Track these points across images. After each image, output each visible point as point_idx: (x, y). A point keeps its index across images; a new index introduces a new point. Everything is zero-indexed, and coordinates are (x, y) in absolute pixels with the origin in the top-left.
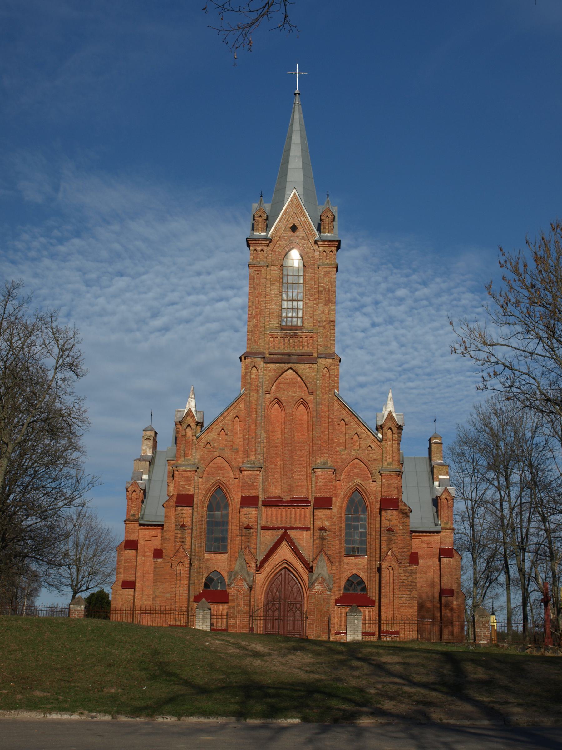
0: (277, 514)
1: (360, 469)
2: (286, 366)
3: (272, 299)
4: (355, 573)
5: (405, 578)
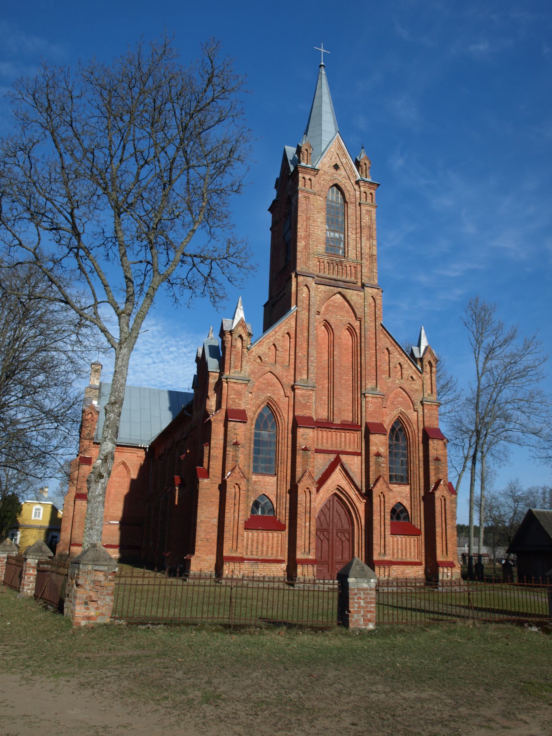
0: (327, 437)
1: (403, 398)
3: (318, 226)
4: (399, 501)
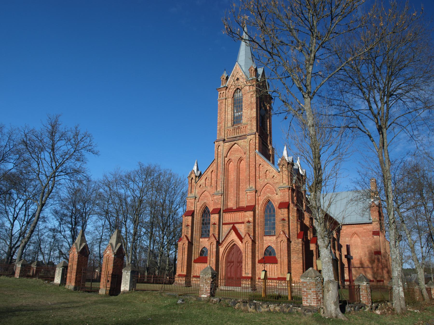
2: (233, 143)
5: (295, 247)
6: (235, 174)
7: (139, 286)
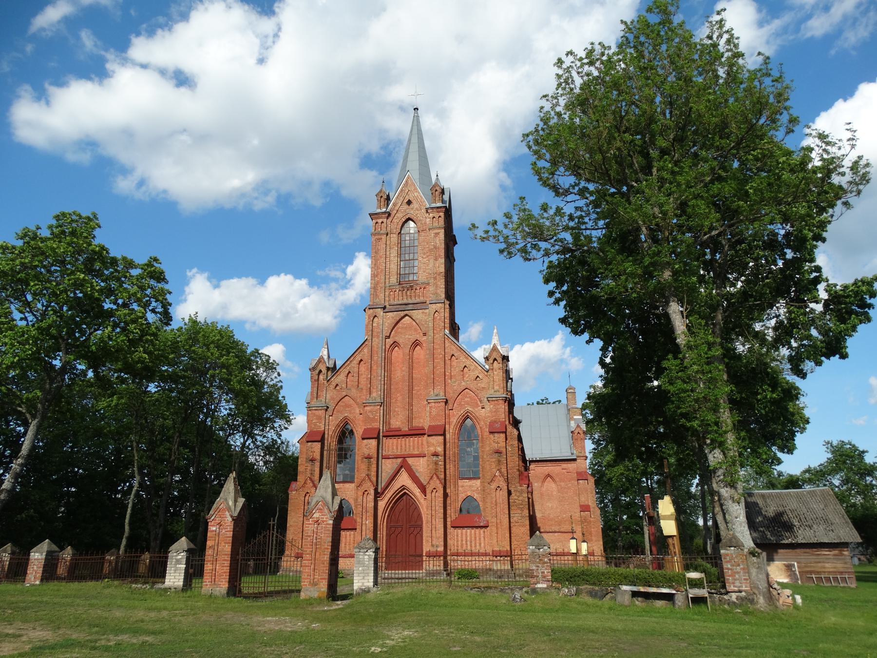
2: (402, 314)
6: (405, 368)
7: (249, 584)
